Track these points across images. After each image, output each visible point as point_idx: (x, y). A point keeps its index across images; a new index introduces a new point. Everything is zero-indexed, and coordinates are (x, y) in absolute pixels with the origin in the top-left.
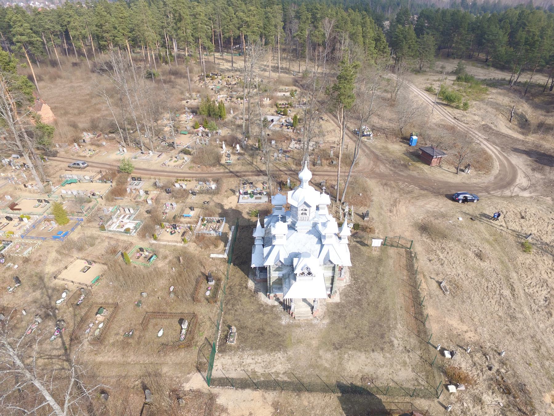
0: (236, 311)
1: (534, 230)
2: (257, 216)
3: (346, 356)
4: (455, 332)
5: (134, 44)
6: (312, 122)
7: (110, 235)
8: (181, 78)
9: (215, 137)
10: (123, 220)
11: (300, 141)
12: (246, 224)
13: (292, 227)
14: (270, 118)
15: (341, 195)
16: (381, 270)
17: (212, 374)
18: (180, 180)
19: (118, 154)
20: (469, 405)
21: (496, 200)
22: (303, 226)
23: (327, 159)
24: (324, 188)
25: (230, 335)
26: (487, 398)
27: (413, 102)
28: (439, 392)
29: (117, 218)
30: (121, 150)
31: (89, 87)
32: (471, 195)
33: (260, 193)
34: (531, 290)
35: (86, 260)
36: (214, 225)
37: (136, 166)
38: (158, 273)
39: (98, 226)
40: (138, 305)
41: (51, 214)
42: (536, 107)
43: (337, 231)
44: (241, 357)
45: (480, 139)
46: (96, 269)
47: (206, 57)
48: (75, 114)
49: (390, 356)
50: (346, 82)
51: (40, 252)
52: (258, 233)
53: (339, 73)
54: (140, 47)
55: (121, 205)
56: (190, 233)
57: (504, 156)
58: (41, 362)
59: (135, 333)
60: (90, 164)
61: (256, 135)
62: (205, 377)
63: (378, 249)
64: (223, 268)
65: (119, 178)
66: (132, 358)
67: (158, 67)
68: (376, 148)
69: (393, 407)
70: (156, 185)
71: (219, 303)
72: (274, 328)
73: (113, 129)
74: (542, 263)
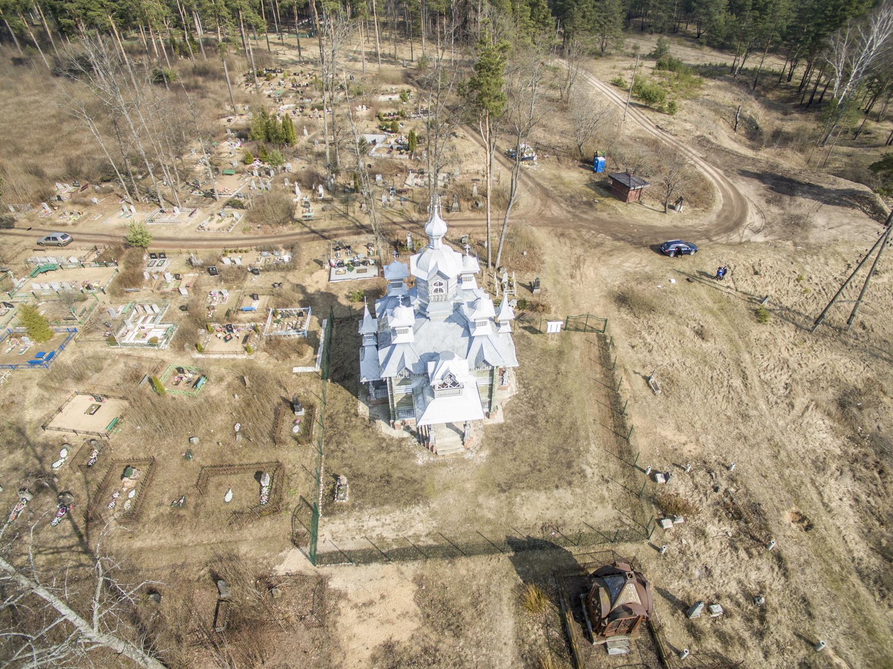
0: (343, 451)
1: (771, 291)
2: (362, 300)
3: (518, 499)
5: (125, 23)
6: (440, 141)
7: (125, 350)
8: (214, 80)
9: (281, 176)
10: (144, 325)
11: (422, 173)
13: (421, 313)
14: (369, 138)
15: (495, 256)
16: (563, 368)
17: (318, 548)
18: (230, 252)
19: (122, 217)
20: (690, 541)
21: (720, 250)
22: (439, 310)
23: (468, 200)
24: (467, 246)
25: (338, 489)
26: (712, 529)
27: (594, 103)
28: (650, 531)
29: (134, 322)
30: (125, 208)
31: (54, 103)
32: (686, 243)
33: (364, 263)
35: (92, 395)
36: (294, 321)
37: (155, 235)
38: (213, 406)
39: (104, 339)
40: (187, 458)
41: (19, 325)
42: (770, 106)
43: (493, 315)
44: (359, 519)
45: (695, 158)
46: (111, 408)
47: (254, 42)
48: (35, 153)
49: (581, 492)
50: (490, 74)
51: (10, 390)
52: (367, 327)
53: (477, 59)
54: (135, 27)
55: (138, 300)
56: (256, 336)
57: (728, 183)
58: (42, 559)
60: (75, 237)
61: (349, 168)
62: (308, 553)
63: (556, 337)
64: (315, 387)
65: (128, 256)
66: (189, 537)
67: (173, 62)
68: (544, 179)
69: (589, 560)
70: (191, 263)
71: (315, 443)
72: (406, 472)
73: (107, 174)
74: (781, 336)
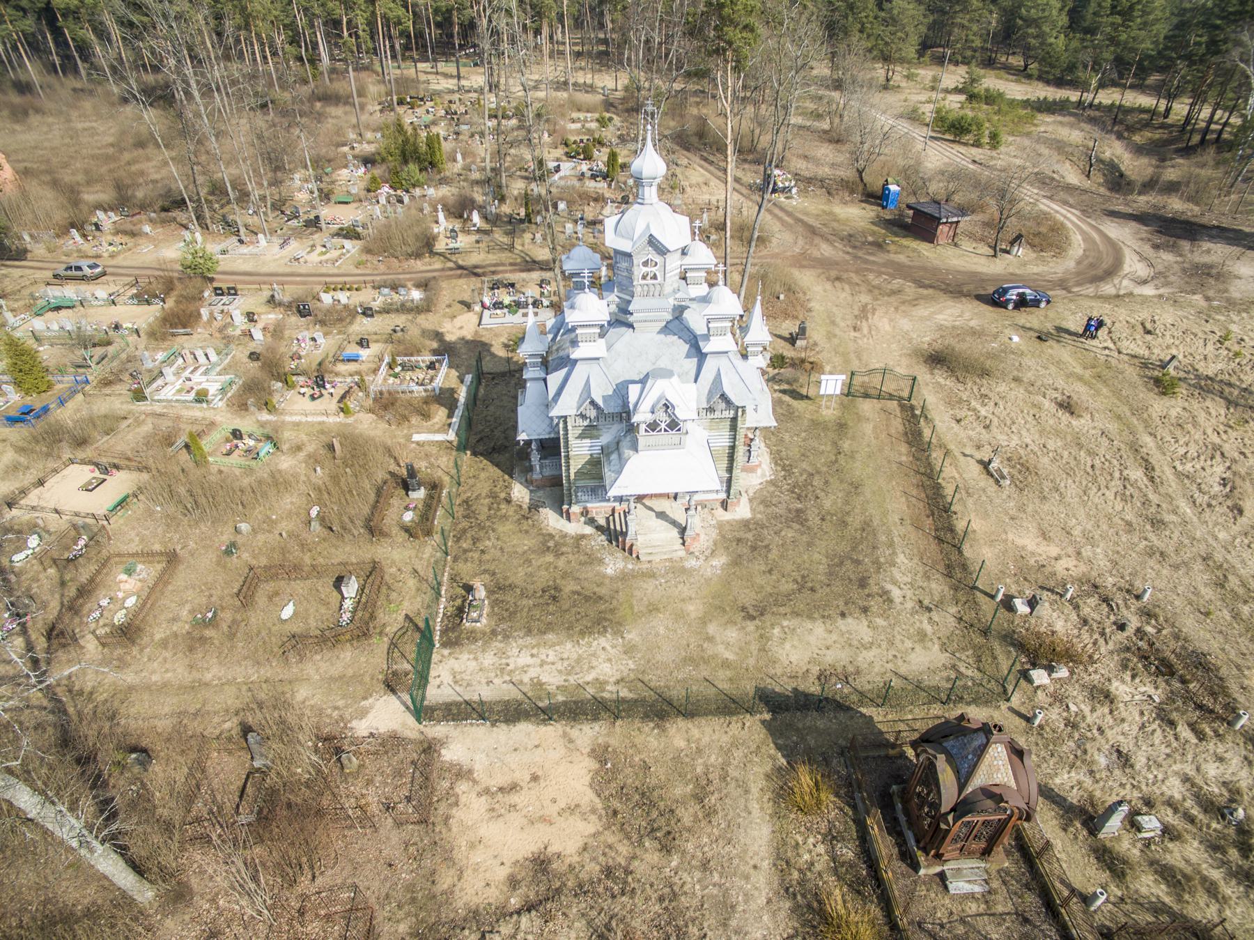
3: (776, 631)
4: (1032, 562)
7: (158, 408)
12: (503, 368)
20: (1083, 706)
26: (1121, 688)
28: (1010, 688)
34: (1188, 467)
35: (97, 465)
38: (279, 483)
40: (228, 552)
44: (502, 653)
57: (1089, 224)
59: (221, 615)
64: (445, 461)
68: (807, 214)
72: (586, 584)
74: (1203, 414)
